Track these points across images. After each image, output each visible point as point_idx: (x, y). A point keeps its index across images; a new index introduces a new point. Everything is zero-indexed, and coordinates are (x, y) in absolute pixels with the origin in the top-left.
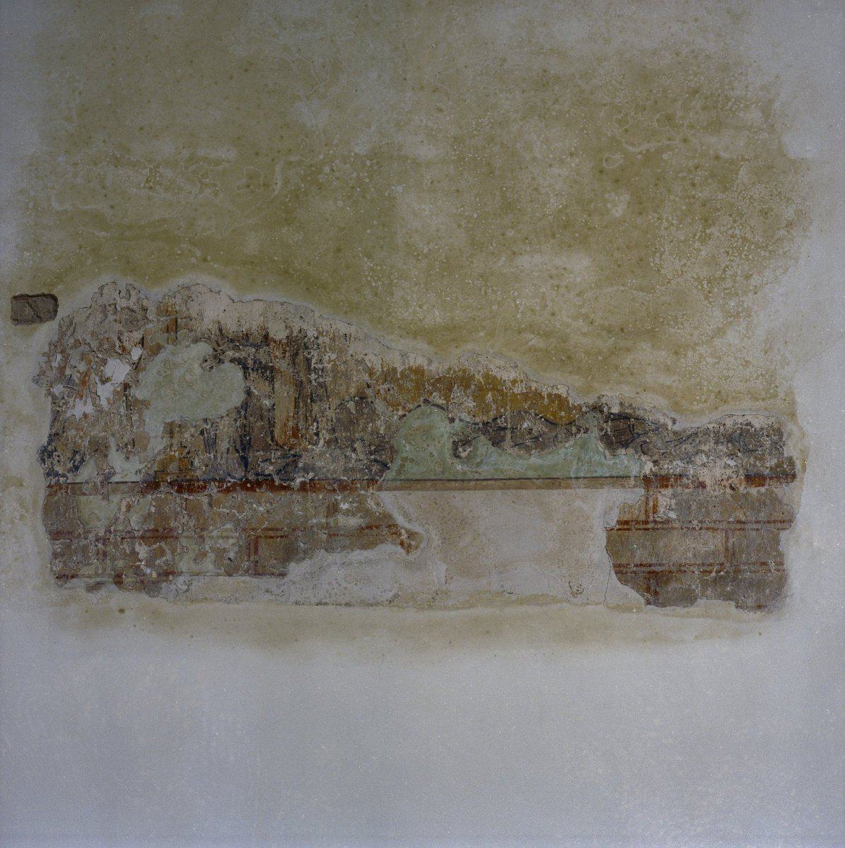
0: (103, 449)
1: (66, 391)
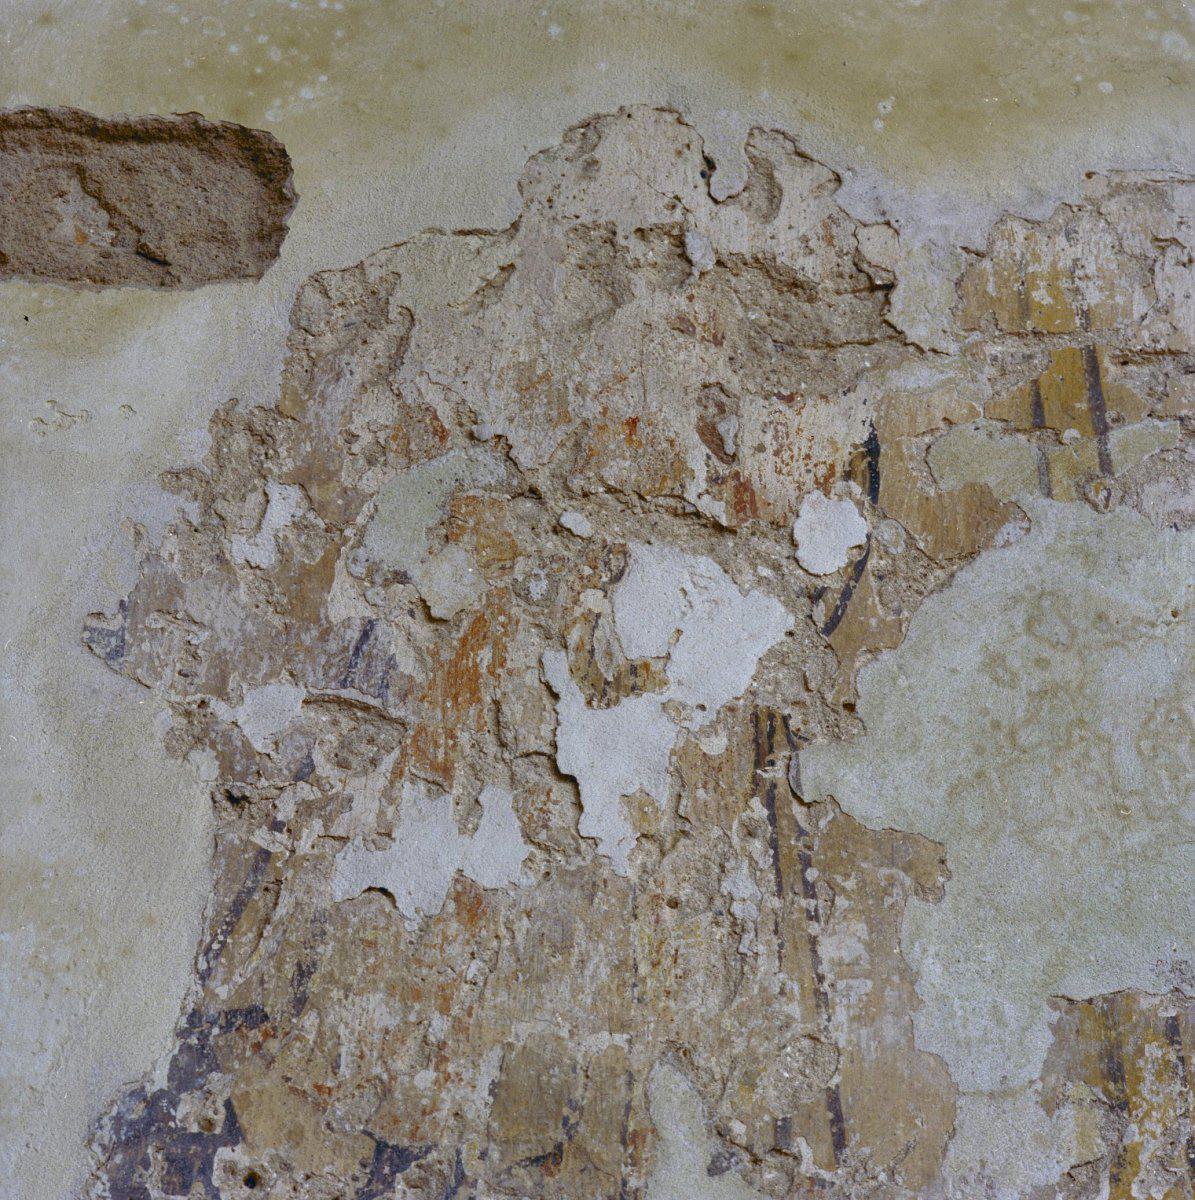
0: (608, 1151)
1: (329, 730)
